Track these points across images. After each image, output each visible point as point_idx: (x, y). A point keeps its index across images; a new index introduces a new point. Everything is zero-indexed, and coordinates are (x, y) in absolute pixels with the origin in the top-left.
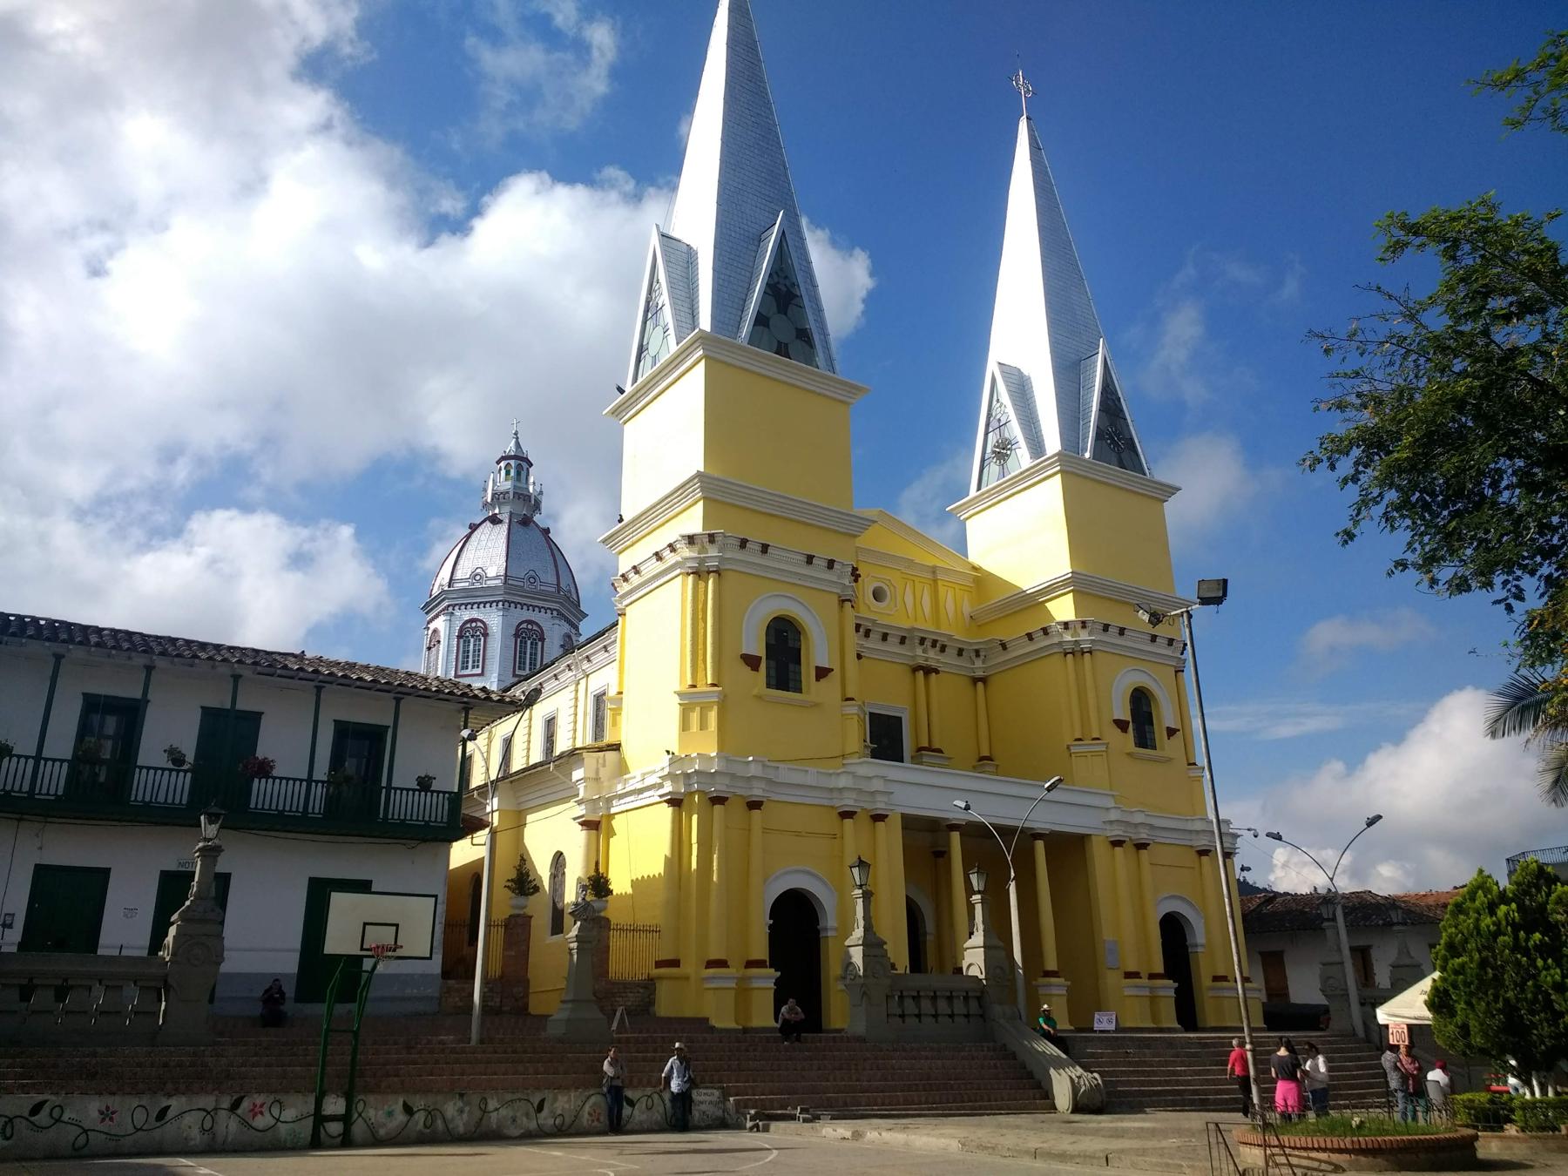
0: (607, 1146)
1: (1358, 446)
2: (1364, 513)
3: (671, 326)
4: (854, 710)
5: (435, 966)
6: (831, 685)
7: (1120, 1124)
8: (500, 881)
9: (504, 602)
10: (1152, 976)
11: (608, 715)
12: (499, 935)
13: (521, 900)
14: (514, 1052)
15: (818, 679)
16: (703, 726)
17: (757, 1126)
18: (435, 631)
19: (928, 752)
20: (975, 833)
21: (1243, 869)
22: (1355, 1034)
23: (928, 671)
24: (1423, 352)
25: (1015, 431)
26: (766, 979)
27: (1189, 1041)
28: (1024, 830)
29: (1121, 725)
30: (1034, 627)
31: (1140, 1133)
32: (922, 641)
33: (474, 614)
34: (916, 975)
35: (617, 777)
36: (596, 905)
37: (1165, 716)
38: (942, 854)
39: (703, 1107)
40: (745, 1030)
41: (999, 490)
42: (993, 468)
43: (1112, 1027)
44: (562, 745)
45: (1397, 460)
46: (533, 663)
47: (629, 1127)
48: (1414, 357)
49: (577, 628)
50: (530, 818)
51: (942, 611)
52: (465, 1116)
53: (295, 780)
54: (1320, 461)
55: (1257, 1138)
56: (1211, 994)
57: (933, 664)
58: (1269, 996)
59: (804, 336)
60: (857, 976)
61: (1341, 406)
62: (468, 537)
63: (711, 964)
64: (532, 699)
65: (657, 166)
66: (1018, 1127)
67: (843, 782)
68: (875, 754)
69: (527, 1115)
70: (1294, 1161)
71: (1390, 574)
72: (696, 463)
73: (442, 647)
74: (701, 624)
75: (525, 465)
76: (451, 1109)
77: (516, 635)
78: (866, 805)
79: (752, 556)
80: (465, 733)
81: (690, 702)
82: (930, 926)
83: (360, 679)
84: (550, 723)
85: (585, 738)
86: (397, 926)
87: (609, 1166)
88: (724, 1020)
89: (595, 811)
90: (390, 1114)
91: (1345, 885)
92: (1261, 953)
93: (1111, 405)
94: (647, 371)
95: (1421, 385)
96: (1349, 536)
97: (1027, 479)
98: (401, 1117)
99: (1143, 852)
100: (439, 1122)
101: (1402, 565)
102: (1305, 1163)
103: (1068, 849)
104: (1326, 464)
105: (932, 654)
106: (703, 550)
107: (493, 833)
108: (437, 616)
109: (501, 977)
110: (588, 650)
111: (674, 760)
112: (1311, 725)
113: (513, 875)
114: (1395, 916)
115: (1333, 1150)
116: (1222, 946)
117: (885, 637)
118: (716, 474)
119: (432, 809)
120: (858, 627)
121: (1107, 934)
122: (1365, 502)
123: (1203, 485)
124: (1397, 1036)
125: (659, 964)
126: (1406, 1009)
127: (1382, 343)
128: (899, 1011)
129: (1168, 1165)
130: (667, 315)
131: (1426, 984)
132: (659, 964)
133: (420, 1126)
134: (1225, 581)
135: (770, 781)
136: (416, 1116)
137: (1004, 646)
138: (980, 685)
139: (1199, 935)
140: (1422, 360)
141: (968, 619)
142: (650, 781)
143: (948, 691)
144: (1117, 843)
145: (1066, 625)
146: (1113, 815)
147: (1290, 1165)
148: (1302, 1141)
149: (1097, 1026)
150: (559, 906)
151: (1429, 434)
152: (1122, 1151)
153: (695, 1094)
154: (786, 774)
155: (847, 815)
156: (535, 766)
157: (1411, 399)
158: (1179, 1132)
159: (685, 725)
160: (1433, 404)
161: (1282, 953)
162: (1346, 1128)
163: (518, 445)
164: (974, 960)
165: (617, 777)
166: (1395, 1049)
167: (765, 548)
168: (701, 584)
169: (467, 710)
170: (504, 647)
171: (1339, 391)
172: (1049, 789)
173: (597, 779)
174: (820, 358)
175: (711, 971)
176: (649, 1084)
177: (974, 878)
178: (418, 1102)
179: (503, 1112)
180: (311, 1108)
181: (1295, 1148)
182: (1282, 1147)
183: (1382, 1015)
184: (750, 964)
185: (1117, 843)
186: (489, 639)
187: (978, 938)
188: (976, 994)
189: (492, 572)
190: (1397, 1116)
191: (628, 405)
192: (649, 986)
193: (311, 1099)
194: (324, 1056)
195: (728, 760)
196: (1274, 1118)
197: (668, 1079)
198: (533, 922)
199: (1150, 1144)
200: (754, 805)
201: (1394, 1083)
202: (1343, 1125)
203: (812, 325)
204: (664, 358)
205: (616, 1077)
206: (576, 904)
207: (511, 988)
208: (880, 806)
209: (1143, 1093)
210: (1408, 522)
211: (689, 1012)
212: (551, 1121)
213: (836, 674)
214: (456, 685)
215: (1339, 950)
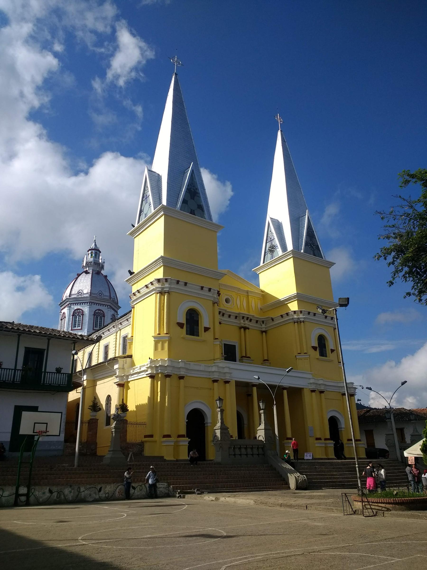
0: (125, 504)
1: (394, 252)
2: (396, 275)
3: (152, 203)
4: (218, 343)
5: (62, 438)
6: (209, 334)
7: (312, 494)
8: (87, 406)
9: (90, 302)
10: (326, 439)
11: (128, 345)
12: (86, 426)
13: (95, 413)
14: (91, 470)
15: (205, 331)
16: (163, 349)
17: (180, 496)
18: (64, 313)
19: (245, 358)
20: (261, 387)
21: (358, 400)
22: (397, 460)
23: (245, 328)
24: (415, 219)
25: (277, 242)
26: (185, 442)
27: (338, 464)
28: (279, 386)
29: (315, 348)
30: (283, 313)
31: (319, 497)
32: (243, 318)
33: (79, 307)
34: (240, 440)
35: (131, 362)
36: (122, 415)
37: (330, 345)
38: (250, 395)
39: (161, 489)
40: (177, 461)
41: (271, 263)
42: (269, 255)
43: (311, 458)
44: (111, 355)
45: (408, 257)
46: (100, 325)
47: (133, 497)
48: (413, 221)
49: (117, 312)
50: (98, 383)
51: (251, 307)
52: (72, 494)
53: (10, 369)
54: (381, 257)
55: (359, 499)
56: (347, 446)
57: (247, 326)
58: (368, 446)
59: (200, 207)
60: (218, 440)
61: (388, 238)
62: (77, 278)
63: (165, 436)
64: (99, 339)
65: (148, 150)
66: (276, 495)
67: (214, 369)
68: (226, 359)
69: (95, 493)
70: (373, 507)
71: (405, 297)
72: (161, 253)
73: (67, 319)
74: (162, 312)
75: (98, 252)
76: (67, 491)
77: (94, 315)
78: (222, 378)
79: (181, 286)
80: (74, 352)
81: (158, 340)
82: (246, 422)
83: (35, 332)
84: (106, 348)
85: (119, 353)
86: (47, 424)
87: (125, 512)
88: (169, 457)
89: (122, 380)
90: (44, 493)
91: (395, 405)
92: (365, 431)
93: (310, 233)
94: (143, 219)
95: (416, 230)
96: (392, 283)
97: (281, 260)
98: (48, 494)
99: (322, 394)
100: (62, 496)
101: (409, 294)
102: (377, 508)
103: (296, 393)
104: (383, 258)
105: (247, 322)
106: (163, 284)
107: (84, 389)
108: (64, 308)
109: (87, 442)
110: (121, 321)
111: (152, 361)
112: (383, 348)
113: (91, 404)
114: (412, 417)
115: (386, 503)
116: (350, 428)
117: (230, 316)
118: (168, 257)
119: (61, 379)
120: (220, 313)
121: (309, 424)
122: (397, 271)
123: (341, 264)
124: (411, 461)
125: (146, 436)
126: (414, 452)
127: (402, 216)
128: (233, 453)
129: (328, 509)
130: (151, 198)
131: (421, 442)
132: (146, 436)
133: (55, 498)
134: (348, 298)
135: (187, 369)
136: (54, 494)
137: (273, 319)
138: (264, 333)
139: (342, 424)
140: (415, 222)
141: (259, 309)
142: (143, 369)
143: (252, 336)
144: (313, 391)
145: (295, 312)
146: (312, 381)
147: (371, 509)
148: (375, 500)
149: (305, 458)
150: (109, 415)
151: (418, 248)
152: (312, 504)
153: (158, 484)
154: (193, 366)
155: (215, 381)
156: (100, 363)
157: (412, 235)
158: (333, 496)
159: (156, 348)
160: (419, 238)
161: (373, 430)
162: (391, 495)
163: (95, 245)
164: (261, 434)
165: (131, 362)
166: (410, 466)
167: (186, 284)
168: (162, 297)
169: (75, 343)
170: (89, 319)
171: (387, 232)
172: (288, 372)
173: (123, 368)
174: (206, 216)
175: (165, 439)
176: (141, 481)
177: (261, 404)
178: (54, 489)
179: (86, 492)
180: (14, 491)
181: (373, 502)
182: (368, 502)
183: (406, 454)
184: (179, 436)
185: (313, 391)
186: (84, 316)
187: (262, 426)
188: (261, 446)
189: (85, 292)
190: (411, 491)
191: (136, 232)
192: (142, 445)
193: (14, 488)
194: (19, 472)
195: (171, 360)
196: (366, 491)
197: (148, 480)
198: (99, 421)
199: (322, 501)
200: (181, 378)
201: (410, 479)
202: (390, 494)
203: (203, 203)
204: (149, 215)
205: (130, 478)
206: (114, 415)
207: (90, 445)
208: (227, 378)
209: (321, 482)
210: (411, 279)
211: (156, 454)
212: (104, 495)
213: (212, 329)
214: (71, 334)
215: (392, 430)
